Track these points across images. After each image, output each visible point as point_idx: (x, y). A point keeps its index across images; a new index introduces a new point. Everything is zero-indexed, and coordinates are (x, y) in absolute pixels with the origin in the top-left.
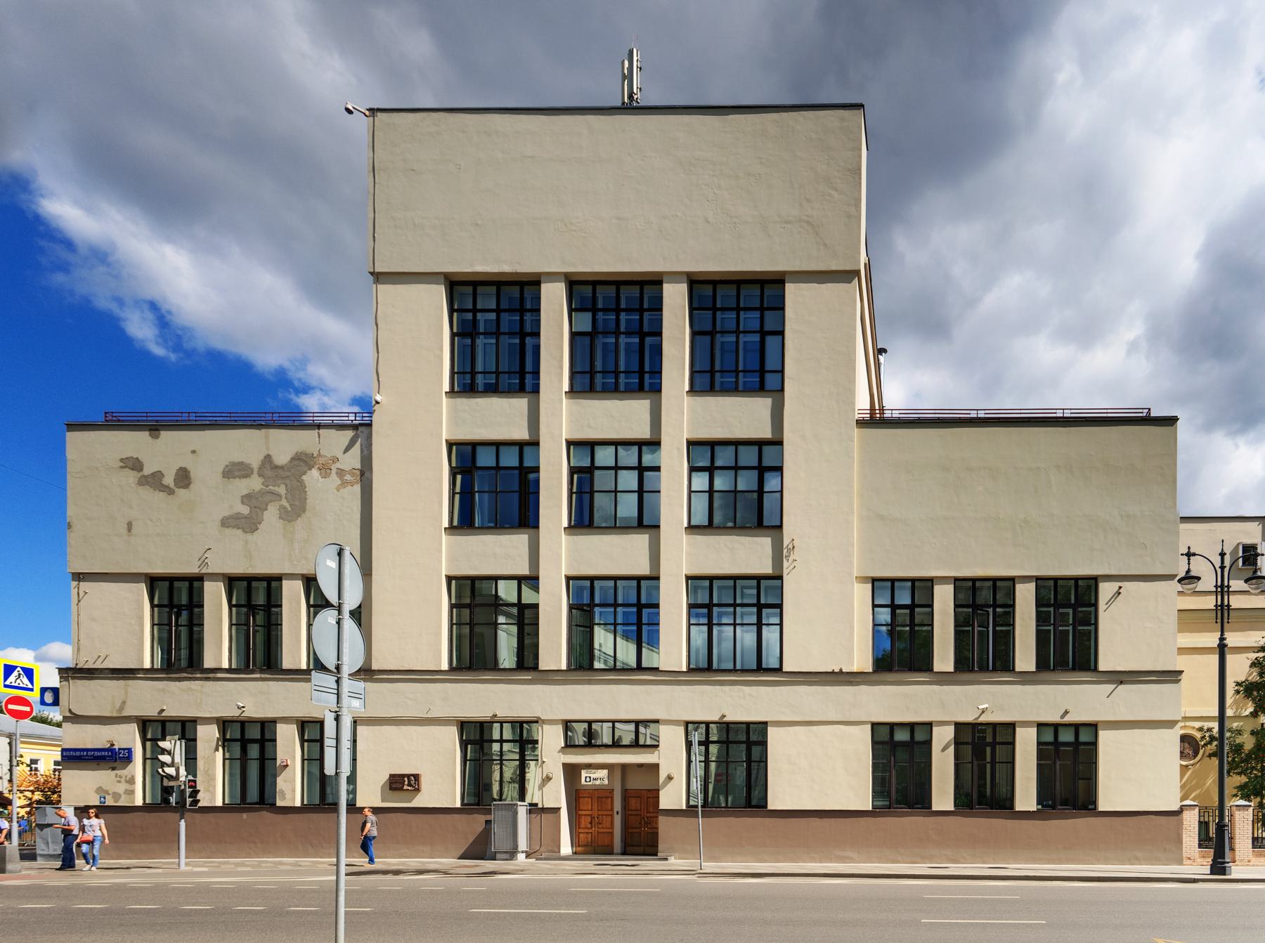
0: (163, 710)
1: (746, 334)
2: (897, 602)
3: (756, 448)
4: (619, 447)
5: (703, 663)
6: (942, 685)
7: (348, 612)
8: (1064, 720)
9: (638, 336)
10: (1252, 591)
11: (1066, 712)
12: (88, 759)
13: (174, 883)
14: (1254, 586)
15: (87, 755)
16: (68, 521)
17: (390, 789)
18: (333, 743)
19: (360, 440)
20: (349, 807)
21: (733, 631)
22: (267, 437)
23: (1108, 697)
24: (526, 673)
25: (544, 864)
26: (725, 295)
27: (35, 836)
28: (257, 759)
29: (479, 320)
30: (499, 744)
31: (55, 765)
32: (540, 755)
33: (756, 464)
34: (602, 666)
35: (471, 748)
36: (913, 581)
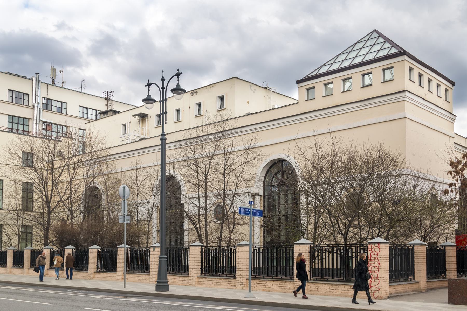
7: (238, 273)
13: (252, 269)
18: (195, 135)
20: (166, 281)
22: (189, 127)
24: (46, 289)
27: (40, 298)
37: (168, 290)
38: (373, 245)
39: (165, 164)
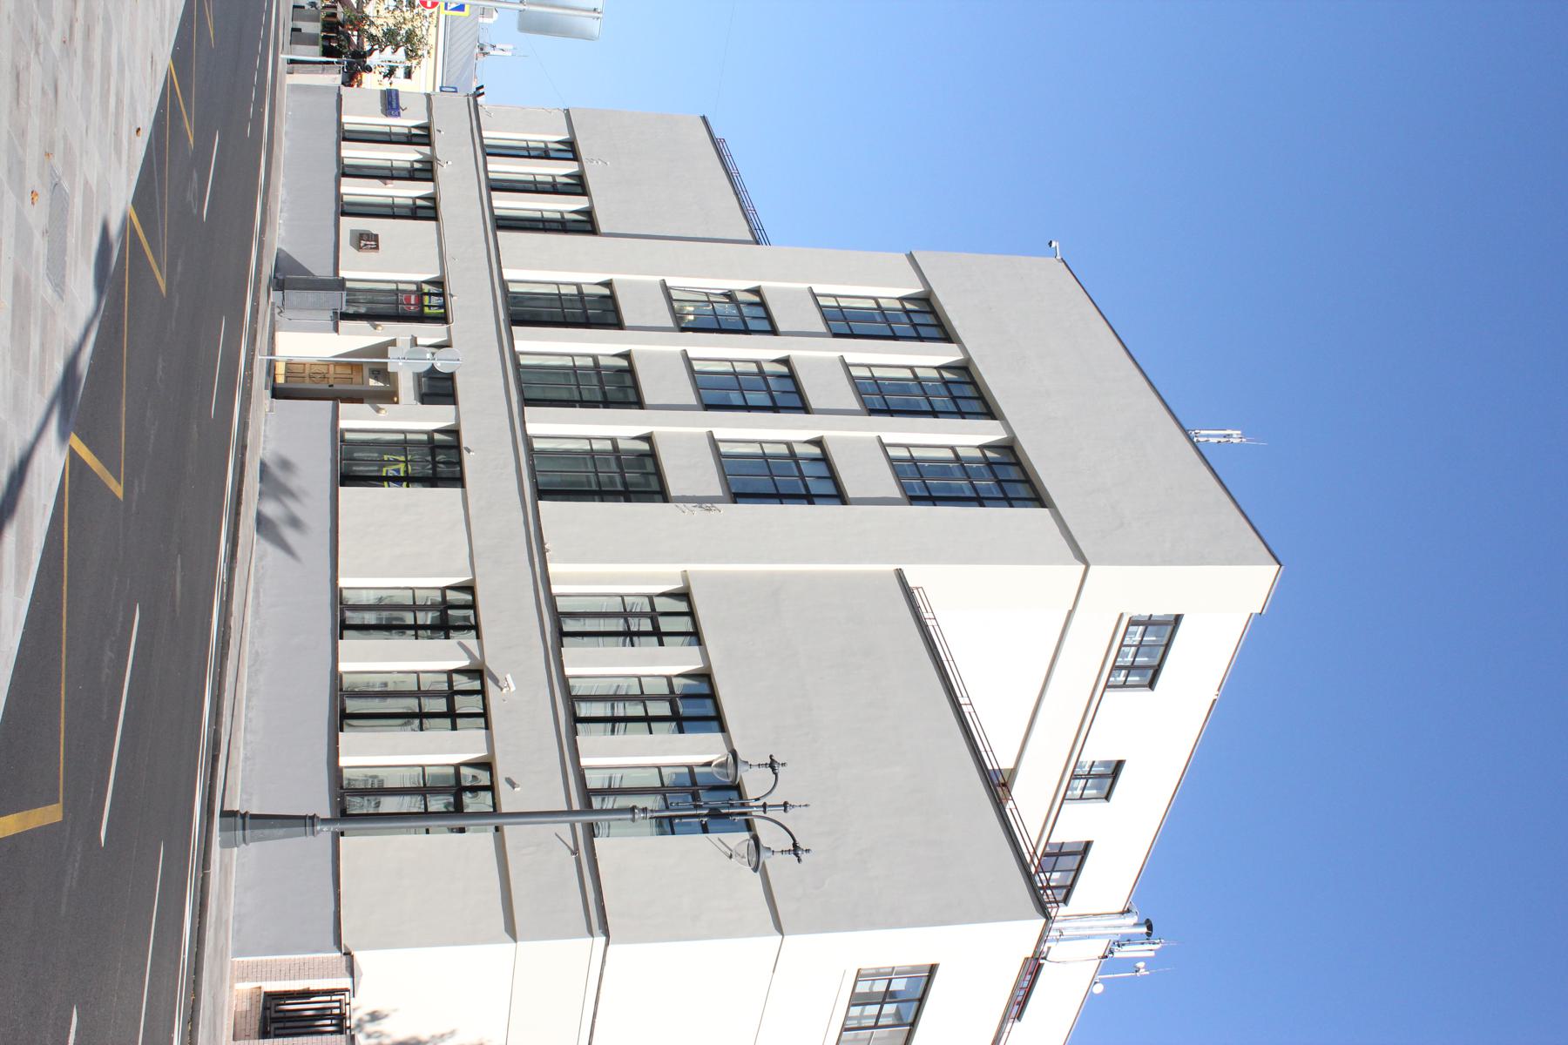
0: (440, 131)
4: (417, 711)
5: (693, 639)
6: (749, 412)
8: (436, 132)
11: (513, 784)
14: (41, 25)
16: (758, 873)
17: (376, 236)
19: (381, 384)
26: (628, 380)
28: (419, 688)
29: (368, 308)
32: (344, 303)
37: (645, 469)
38: (962, 701)
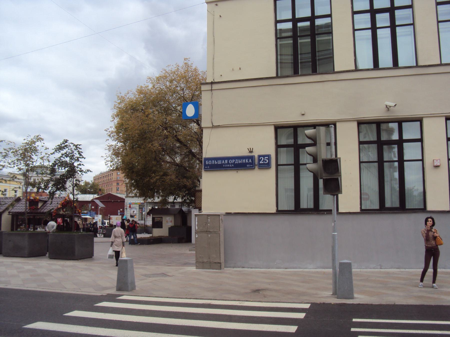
1: (281, 40)
2: (299, 15)
3: (421, 158)
9: (310, 37)
10: (80, 152)
12: (229, 167)
15: (228, 163)
21: (284, 163)
23: (248, 149)
25: (206, 271)
30: (387, 15)
31: (33, 190)
33: (368, 8)
34: (391, 125)
35: (307, 42)
36: (277, 38)
39: (312, 61)
